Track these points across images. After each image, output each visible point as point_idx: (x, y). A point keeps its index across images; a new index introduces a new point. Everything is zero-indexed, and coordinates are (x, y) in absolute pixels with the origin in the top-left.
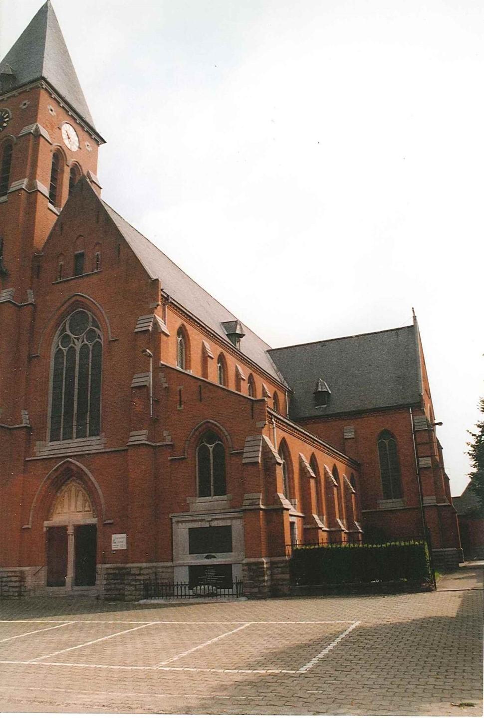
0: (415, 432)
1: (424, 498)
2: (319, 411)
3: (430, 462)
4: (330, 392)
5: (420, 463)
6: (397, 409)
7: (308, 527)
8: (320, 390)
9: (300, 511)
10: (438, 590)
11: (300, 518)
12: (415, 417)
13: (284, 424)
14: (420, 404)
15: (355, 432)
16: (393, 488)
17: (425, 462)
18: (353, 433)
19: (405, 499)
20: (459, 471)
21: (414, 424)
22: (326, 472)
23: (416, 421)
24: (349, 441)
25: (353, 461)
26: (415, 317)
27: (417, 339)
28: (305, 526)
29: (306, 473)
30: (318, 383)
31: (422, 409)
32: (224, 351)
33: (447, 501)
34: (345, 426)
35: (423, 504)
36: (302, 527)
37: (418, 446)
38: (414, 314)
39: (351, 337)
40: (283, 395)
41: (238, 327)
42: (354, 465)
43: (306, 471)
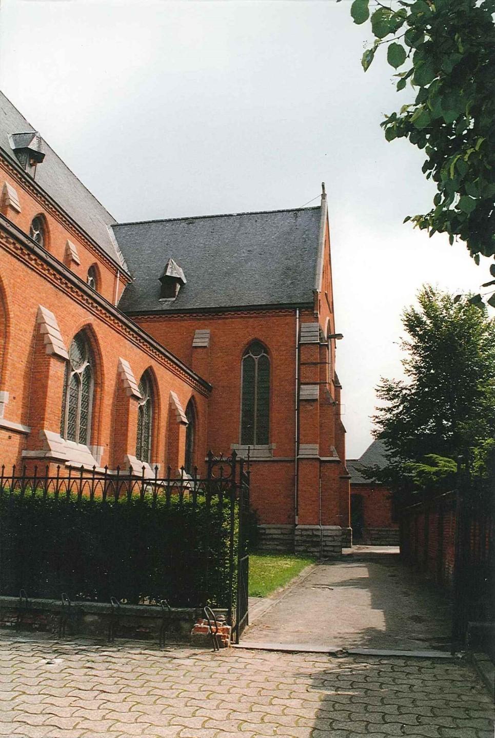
0: (300, 345)
1: (302, 446)
2: (167, 304)
3: (318, 392)
4: (185, 281)
5: (301, 393)
6: (277, 309)
7: (32, 454)
8: (168, 274)
9: (19, 420)
10: (242, 644)
11: (22, 436)
12: (302, 324)
13: (177, 368)
14: (312, 305)
15: (211, 339)
16: (256, 428)
17: (310, 391)
18: (207, 340)
19: (274, 446)
20: (361, 422)
21: (299, 335)
22: (120, 370)
23: (303, 330)
24: (200, 350)
25: (202, 382)
26: (324, 196)
27: (324, 215)
28: (24, 453)
29: (44, 347)
30: (168, 264)
31: (315, 312)
32: (98, 262)
33: (335, 453)
34: (197, 329)
35: (298, 455)
36: (20, 452)
37: (302, 367)
38: (324, 192)
39: (231, 215)
40: (112, 277)
41: (35, 140)
42: (203, 387)
43: (45, 342)
